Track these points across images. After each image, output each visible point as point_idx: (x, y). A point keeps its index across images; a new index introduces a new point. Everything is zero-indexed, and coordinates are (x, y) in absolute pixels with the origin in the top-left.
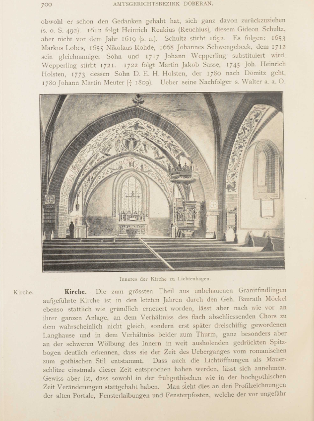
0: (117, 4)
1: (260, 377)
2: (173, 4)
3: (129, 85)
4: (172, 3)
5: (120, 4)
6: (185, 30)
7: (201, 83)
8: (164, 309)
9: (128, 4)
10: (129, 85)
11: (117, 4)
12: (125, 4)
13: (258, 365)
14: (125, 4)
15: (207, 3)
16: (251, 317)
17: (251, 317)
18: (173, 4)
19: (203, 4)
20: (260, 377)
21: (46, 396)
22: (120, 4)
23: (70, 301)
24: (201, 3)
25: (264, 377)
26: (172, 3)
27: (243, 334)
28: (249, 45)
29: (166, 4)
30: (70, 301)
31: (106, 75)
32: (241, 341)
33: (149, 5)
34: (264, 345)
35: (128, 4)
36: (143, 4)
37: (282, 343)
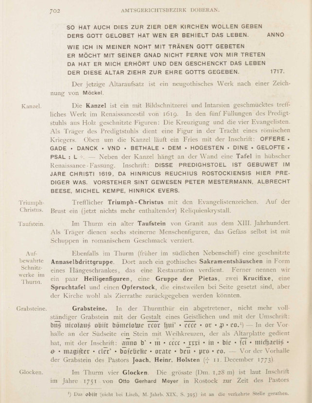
0: (125, 10)
1: (172, 262)
2: (180, 10)
3: (206, 362)
4: (179, 10)
5: (127, 11)
6: (161, 270)
7: (205, 254)
8: (286, 223)
9: (136, 10)
10: (206, 362)
11: (125, 10)
12: (162, 10)
13: (96, 60)
14: (133, 10)
15: (213, 10)
16: (188, 203)
17: (167, 233)
18: (180, 10)
19: (210, 10)
20: (172, 262)
21: (53, 296)
22: (127, 11)
23: (38, 261)
24: (207, 10)
25: (176, 262)
26: (179, 10)
27: (210, 288)
28: (165, 239)
29: (173, 10)
30: (38, 261)
31: (284, 334)
32: (278, 111)
33: (156, 11)
34: (77, 243)
35: (136, 10)
36: (150, 10)
37: (38, 268)
